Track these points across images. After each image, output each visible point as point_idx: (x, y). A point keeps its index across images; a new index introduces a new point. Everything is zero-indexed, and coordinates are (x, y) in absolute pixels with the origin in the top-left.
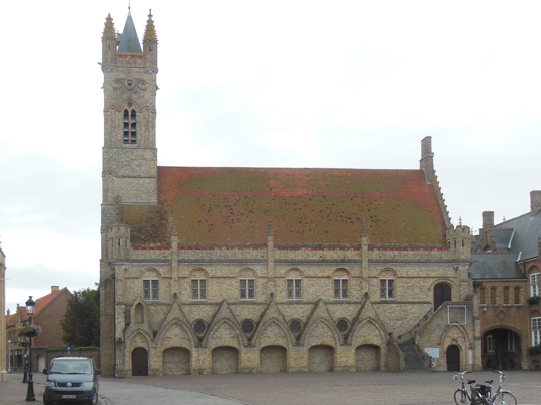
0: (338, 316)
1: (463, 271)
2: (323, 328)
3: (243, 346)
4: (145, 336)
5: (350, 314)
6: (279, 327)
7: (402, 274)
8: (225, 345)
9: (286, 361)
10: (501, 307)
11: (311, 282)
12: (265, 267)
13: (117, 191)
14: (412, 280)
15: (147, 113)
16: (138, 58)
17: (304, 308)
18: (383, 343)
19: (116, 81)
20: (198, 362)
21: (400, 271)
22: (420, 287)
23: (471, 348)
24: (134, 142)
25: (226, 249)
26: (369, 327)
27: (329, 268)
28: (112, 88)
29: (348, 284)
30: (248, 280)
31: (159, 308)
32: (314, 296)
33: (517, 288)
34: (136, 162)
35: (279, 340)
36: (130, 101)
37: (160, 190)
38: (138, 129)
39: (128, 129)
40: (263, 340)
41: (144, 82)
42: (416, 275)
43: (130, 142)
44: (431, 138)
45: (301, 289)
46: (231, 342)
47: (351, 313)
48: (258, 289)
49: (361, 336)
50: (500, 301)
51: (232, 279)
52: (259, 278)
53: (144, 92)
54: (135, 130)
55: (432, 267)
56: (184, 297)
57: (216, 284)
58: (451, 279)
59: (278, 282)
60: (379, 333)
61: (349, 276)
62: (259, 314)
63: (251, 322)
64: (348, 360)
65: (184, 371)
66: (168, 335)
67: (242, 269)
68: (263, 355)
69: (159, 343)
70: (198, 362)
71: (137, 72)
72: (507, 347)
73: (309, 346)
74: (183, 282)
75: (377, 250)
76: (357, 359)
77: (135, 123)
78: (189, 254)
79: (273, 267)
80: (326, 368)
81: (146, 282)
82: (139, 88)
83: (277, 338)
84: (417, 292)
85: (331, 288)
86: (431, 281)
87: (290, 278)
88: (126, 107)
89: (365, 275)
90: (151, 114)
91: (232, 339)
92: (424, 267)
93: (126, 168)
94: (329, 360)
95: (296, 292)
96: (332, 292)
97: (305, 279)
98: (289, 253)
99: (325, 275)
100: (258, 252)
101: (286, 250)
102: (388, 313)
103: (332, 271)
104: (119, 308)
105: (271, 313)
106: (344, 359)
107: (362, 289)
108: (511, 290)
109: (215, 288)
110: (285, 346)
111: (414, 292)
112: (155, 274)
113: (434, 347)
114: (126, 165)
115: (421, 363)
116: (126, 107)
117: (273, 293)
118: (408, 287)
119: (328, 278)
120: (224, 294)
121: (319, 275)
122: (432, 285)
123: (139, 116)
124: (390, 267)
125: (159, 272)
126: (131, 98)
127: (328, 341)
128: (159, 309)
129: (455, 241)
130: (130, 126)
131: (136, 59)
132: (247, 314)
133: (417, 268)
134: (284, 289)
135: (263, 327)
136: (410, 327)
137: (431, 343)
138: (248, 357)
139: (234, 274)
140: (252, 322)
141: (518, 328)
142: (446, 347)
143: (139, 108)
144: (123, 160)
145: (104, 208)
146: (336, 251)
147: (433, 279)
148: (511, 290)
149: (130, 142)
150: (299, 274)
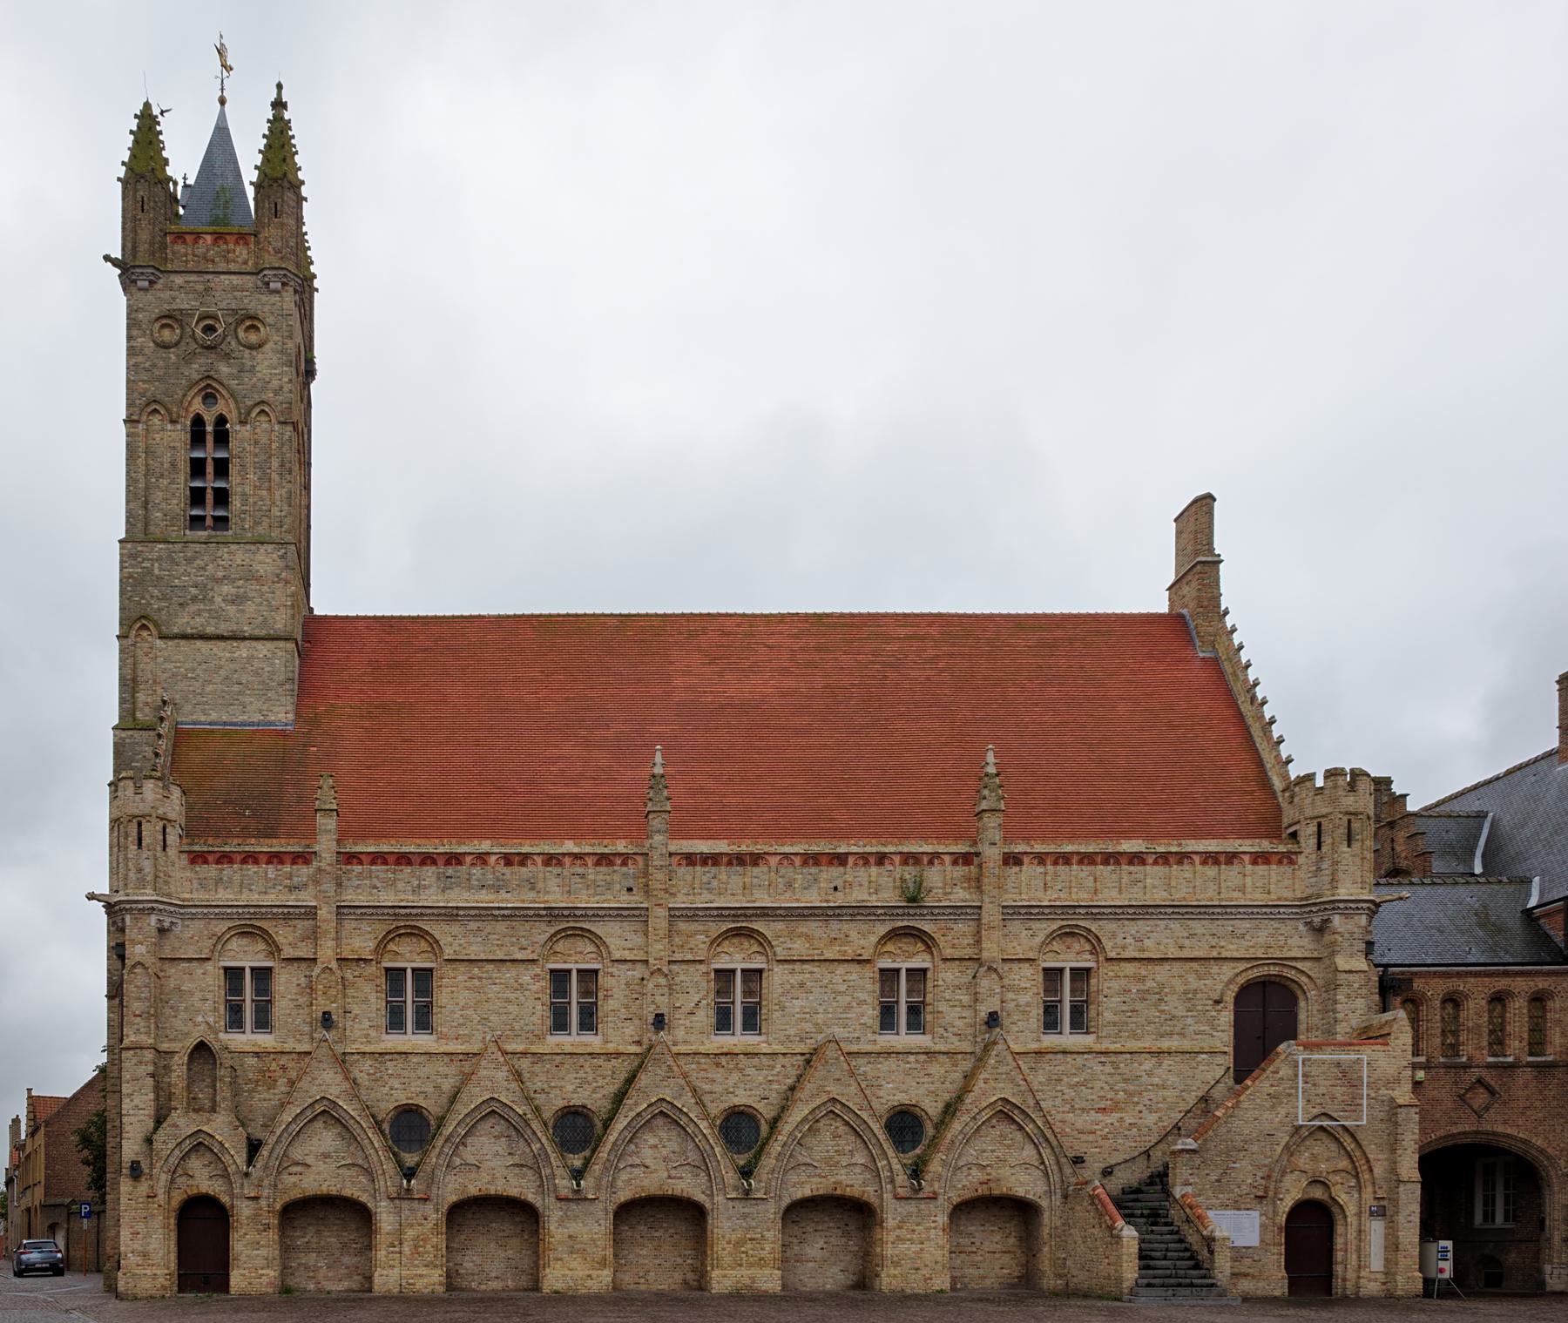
0: (891, 1097)
1: (1347, 936)
2: (836, 1136)
3: (553, 1199)
4: (220, 1159)
5: (932, 1088)
6: (682, 1132)
7: (1124, 948)
8: (493, 1192)
9: (705, 1252)
10: (1478, 1066)
11: (798, 978)
12: (638, 926)
13: (165, 685)
14: (1158, 968)
15: (265, 426)
16: (237, 243)
17: (773, 1067)
18: (1050, 1193)
19: (164, 321)
20: (397, 1249)
21: (1114, 935)
22: (1185, 993)
23: (1381, 1212)
24: (222, 522)
25: (502, 862)
26: (1001, 1136)
27: (865, 927)
28: (151, 344)
29: (929, 984)
30: (579, 971)
31: (274, 1064)
32: (808, 1026)
33: (1538, 1000)
34: (226, 589)
35: (681, 1178)
36: (209, 386)
37: (306, 687)
38: (234, 481)
39: (205, 482)
40: (624, 1176)
41: (256, 323)
42: (1173, 952)
43: (209, 522)
44: (1215, 500)
45: (764, 1003)
46: (513, 1181)
47: (938, 1085)
48: (610, 1001)
49: (969, 1166)
50: (1474, 1048)
51: (522, 967)
52: (616, 964)
53: (254, 353)
54: (228, 482)
55: (1231, 922)
56: (356, 1026)
57: (467, 984)
58: (1299, 965)
59: (682, 978)
60: (1037, 1156)
61: (932, 954)
62: (775, 1092)
63: (586, 1116)
64: (922, 1250)
65: (356, 1277)
66: (297, 1153)
67: (559, 932)
68: (627, 1228)
69: (266, 1183)
70: (397, 1249)
71: (234, 288)
72: (1471, 1214)
73: (786, 1202)
74: (356, 974)
75: (1036, 861)
76: (953, 1249)
77: (228, 459)
78: (377, 877)
79: (664, 924)
80: (841, 1276)
81: (233, 976)
82: (240, 343)
83: (673, 1173)
84: (1175, 1012)
85: (870, 1000)
86: (1227, 971)
87: (723, 963)
88: (197, 406)
89: (990, 950)
90: (277, 427)
91: (517, 1171)
92: (1203, 922)
93: (193, 608)
94: (857, 1248)
95: (744, 1014)
96: (871, 1014)
97: (778, 969)
98: (723, 877)
99: (850, 952)
100: (614, 871)
101: (713, 865)
102: (1071, 1086)
103: (874, 939)
104: (134, 1061)
105: (654, 1087)
106: (909, 1249)
107: (976, 1000)
108: (1518, 1008)
109: (464, 997)
110: (700, 1197)
111: (1162, 1012)
112: (261, 946)
113: (1243, 1206)
114: (194, 599)
115: (1197, 1266)
116: (197, 406)
117: (662, 1015)
118: (1143, 995)
119: (859, 962)
120: (493, 1018)
121: (829, 955)
122: (1231, 987)
123: (240, 435)
124: (1080, 923)
125: (274, 942)
126: (212, 373)
127: (854, 1182)
128: (274, 1066)
129: (1319, 825)
130: (210, 469)
131: (231, 246)
132: (570, 1088)
133: (1175, 925)
134: (704, 1002)
135: (626, 1133)
136: (1148, 1138)
137: (1232, 1191)
138: (570, 1237)
139: (530, 949)
140: (591, 1114)
141: (1539, 1142)
142: (1287, 1210)
143: (238, 408)
144: (185, 581)
145: (123, 739)
146: (891, 868)
147: (1235, 964)
148: (1518, 1008)
149: (209, 522)
150: (756, 948)
